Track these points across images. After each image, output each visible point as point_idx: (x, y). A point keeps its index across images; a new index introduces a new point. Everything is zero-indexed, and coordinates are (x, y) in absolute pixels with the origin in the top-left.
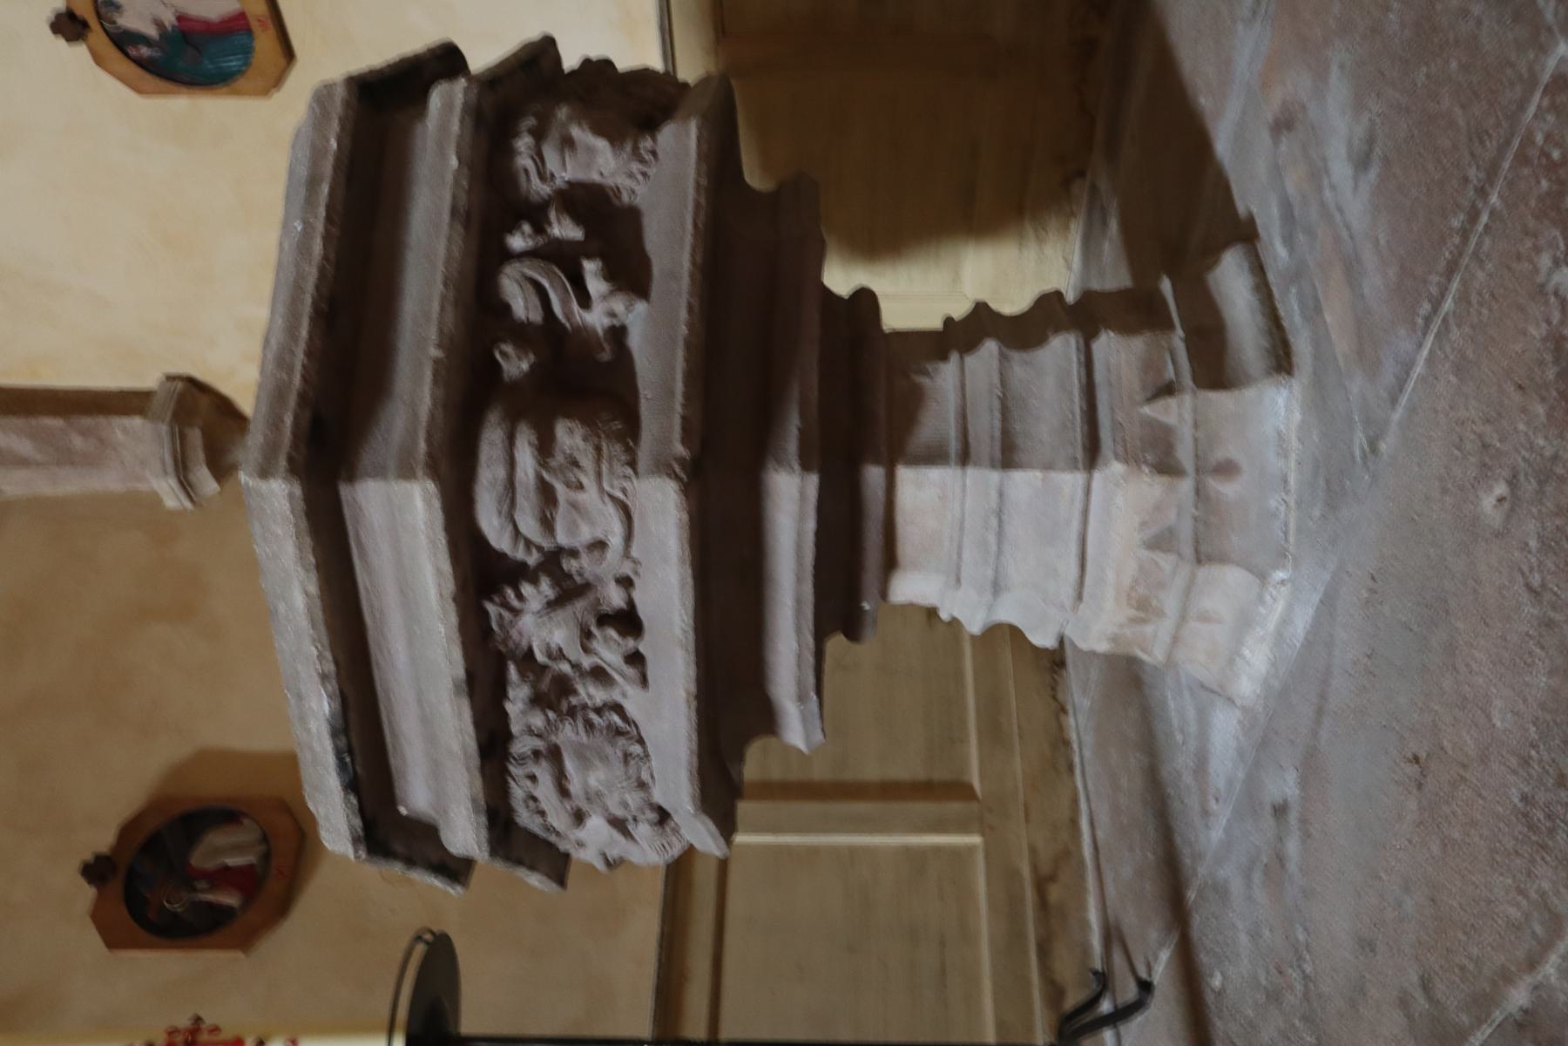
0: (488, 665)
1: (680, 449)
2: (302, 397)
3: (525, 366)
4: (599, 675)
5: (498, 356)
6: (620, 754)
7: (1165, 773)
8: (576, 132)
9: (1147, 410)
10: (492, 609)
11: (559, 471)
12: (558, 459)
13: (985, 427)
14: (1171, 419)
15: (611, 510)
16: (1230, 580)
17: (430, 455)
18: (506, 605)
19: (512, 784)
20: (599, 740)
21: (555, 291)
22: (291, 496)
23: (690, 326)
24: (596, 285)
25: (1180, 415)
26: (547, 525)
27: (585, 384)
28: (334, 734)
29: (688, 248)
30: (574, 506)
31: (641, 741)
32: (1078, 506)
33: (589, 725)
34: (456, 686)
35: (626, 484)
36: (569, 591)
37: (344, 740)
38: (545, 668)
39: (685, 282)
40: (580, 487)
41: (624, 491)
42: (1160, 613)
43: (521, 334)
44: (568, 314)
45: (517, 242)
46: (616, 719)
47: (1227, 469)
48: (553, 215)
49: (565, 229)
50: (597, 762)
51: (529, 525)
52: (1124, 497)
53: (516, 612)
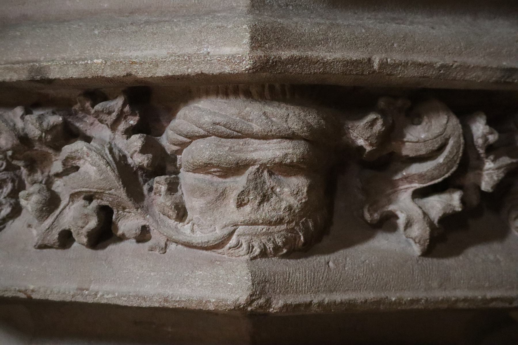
1: (277, 304)
3: (361, 142)
4: (51, 203)
5: (372, 116)
10: (117, 104)
11: (256, 182)
15: (219, 233)
17: (278, 62)
18: (121, 116)
21: (435, 168)
23: (399, 302)
24: (437, 205)
26: (204, 168)
27: (340, 192)
29: (470, 294)
30: (223, 195)
34: (39, 70)
36: (132, 181)
38: (58, 149)
39: (440, 295)
40: (240, 204)
41: (238, 245)
43: (391, 135)
44: (408, 179)
45: (480, 128)
48: (506, 160)
51: (202, 150)
53: (113, 127)
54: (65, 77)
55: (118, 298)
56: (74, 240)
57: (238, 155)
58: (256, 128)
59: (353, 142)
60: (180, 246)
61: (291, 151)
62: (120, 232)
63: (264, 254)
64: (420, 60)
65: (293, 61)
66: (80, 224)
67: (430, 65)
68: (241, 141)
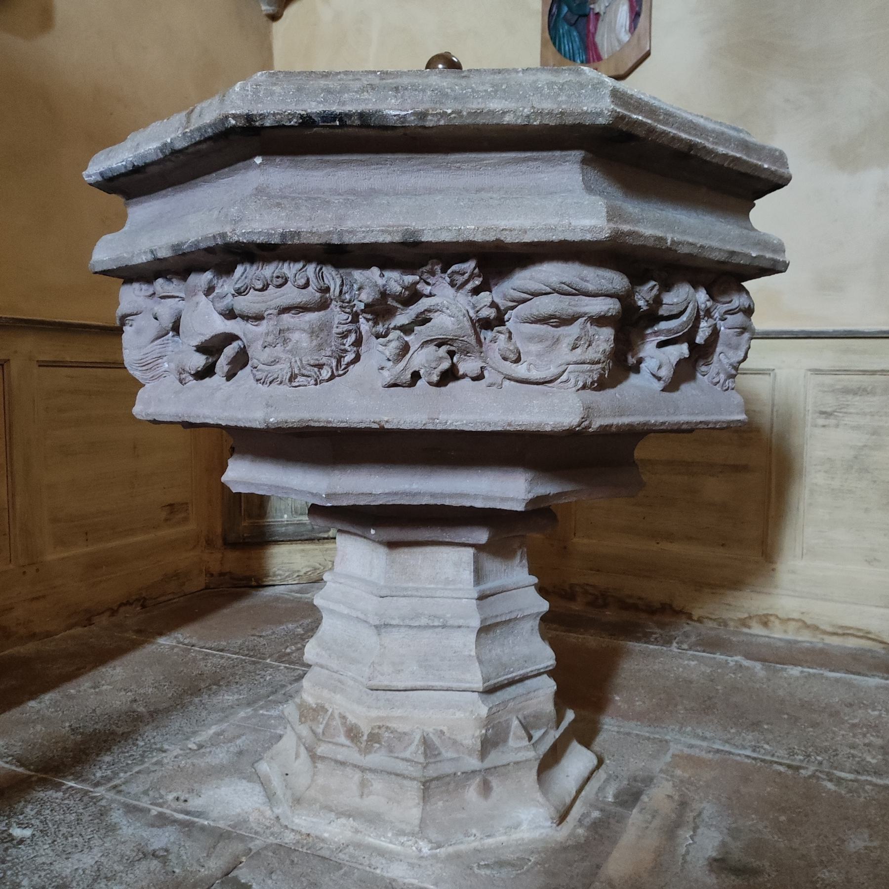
0: (413, 255)
1: (595, 425)
2: (651, 130)
3: (641, 303)
5: (653, 283)
6: (324, 360)
7: (150, 735)
9: (516, 722)
12: (592, 329)
13: (500, 608)
14: (512, 742)
15: (553, 371)
16: (410, 809)
18: (472, 277)
19: (299, 265)
22: (600, 114)
30: (557, 341)
31: (332, 377)
32: (455, 685)
33: (344, 335)
34: (414, 233)
35: (573, 381)
37: (357, 122)
40: (574, 348)
41: (567, 381)
42: (367, 751)
44: (656, 333)
46: (349, 357)
47: (486, 789)
50: (315, 343)
52: (460, 716)
54: (437, 240)
55: (466, 424)
56: (420, 378)
57: (575, 309)
58: (591, 287)
59: (635, 302)
60: (512, 383)
61: (612, 306)
62: (461, 373)
63: (584, 387)
65: (630, 234)
66: (434, 365)
68: (576, 298)
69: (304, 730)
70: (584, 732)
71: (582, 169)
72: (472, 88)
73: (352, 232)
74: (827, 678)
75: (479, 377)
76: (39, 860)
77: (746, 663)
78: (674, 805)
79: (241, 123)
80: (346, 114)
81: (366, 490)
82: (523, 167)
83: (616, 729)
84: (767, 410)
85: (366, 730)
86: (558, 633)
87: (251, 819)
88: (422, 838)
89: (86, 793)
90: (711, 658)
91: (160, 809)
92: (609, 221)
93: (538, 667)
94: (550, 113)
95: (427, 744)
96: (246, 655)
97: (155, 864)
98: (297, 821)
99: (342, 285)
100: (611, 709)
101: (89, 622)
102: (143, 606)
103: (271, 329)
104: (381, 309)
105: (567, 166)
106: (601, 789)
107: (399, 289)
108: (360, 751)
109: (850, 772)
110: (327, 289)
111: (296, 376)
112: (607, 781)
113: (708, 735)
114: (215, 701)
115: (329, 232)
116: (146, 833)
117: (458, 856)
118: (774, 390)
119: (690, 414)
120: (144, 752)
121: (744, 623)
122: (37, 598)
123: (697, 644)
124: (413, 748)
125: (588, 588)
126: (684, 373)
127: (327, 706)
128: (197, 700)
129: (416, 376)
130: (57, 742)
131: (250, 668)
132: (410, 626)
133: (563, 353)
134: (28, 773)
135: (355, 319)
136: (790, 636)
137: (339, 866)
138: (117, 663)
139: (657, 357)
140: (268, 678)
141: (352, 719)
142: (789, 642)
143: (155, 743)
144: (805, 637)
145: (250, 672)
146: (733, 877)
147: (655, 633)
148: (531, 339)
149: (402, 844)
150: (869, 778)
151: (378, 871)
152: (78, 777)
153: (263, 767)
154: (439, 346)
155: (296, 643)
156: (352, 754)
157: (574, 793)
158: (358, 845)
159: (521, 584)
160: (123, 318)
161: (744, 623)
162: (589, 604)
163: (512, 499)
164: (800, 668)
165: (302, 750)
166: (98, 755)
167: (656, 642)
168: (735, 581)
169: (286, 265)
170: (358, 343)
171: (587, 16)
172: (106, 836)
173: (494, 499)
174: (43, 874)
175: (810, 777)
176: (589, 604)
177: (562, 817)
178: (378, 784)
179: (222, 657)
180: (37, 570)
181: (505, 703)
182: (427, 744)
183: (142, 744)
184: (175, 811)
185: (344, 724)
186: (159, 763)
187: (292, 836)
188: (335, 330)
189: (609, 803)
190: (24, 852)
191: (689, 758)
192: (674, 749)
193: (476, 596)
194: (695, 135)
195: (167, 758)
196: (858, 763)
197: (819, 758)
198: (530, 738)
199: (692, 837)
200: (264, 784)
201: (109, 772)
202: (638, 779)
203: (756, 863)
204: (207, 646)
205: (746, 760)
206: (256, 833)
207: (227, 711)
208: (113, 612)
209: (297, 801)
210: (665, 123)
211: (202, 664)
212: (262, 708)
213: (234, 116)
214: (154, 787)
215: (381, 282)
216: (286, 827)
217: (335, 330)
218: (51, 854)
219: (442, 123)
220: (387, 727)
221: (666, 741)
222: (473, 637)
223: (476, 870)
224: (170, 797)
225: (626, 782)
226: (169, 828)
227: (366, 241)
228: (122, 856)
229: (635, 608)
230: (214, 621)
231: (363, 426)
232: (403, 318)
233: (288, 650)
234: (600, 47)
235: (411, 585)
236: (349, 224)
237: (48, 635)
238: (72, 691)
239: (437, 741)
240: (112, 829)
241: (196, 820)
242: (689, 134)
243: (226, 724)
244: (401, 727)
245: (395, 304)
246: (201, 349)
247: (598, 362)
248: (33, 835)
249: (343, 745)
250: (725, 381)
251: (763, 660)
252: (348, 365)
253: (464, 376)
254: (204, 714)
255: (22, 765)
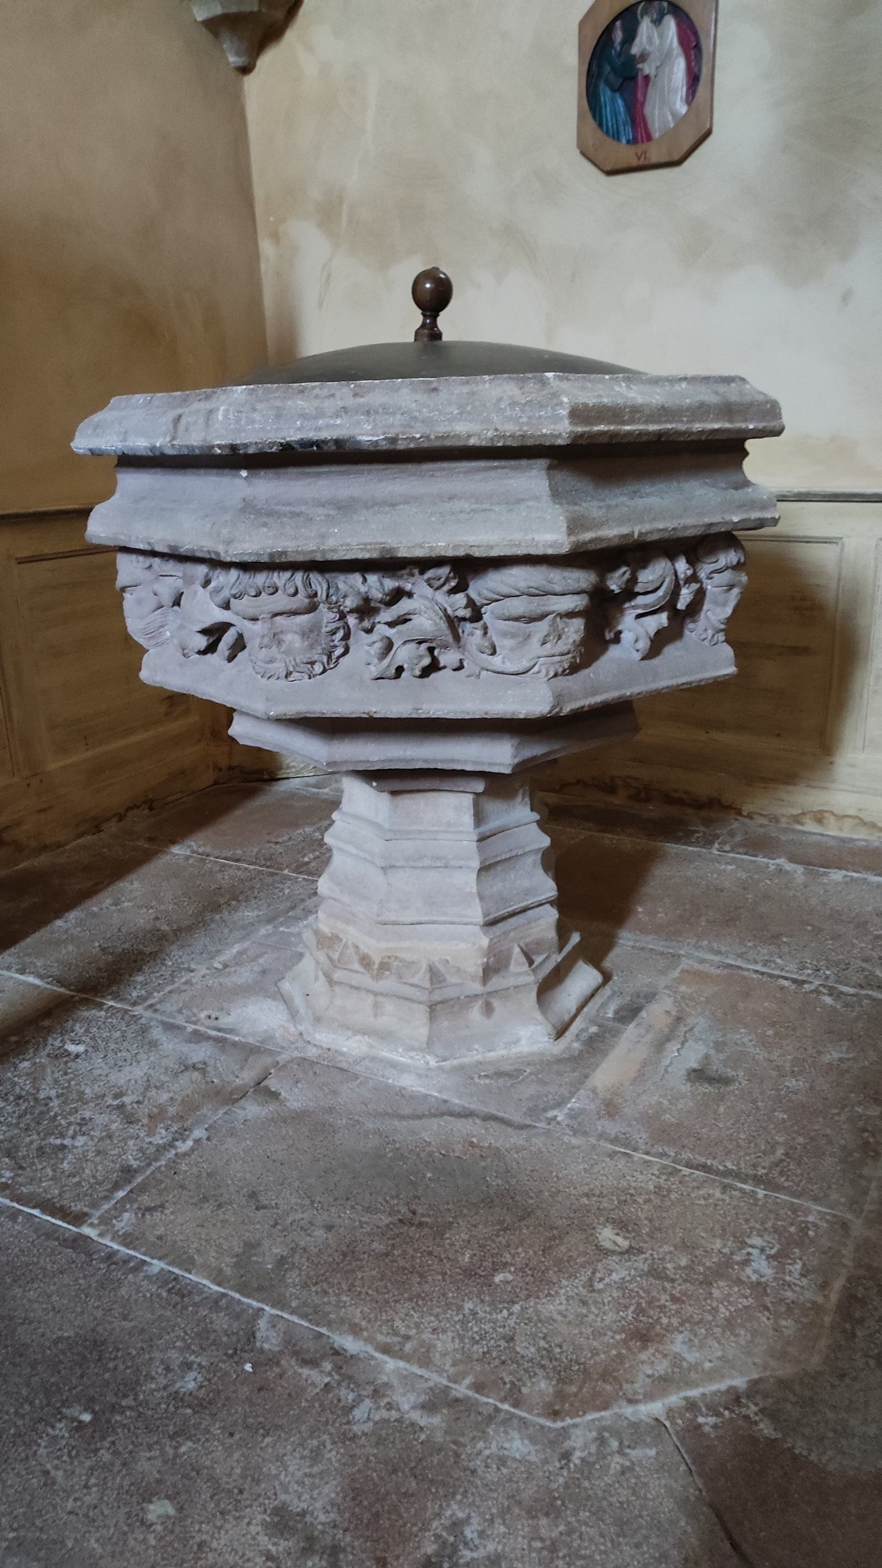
1: (567, 709)
3: (613, 587)
5: (624, 569)
6: (316, 657)
7: (176, 955)
8: (736, 591)
9: (517, 950)
11: (553, 623)
13: (499, 847)
14: (513, 968)
15: (525, 664)
16: (418, 1027)
18: (447, 580)
19: (287, 575)
20: (324, 641)
25: (520, 974)
28: (337, 442)
30: (529, 636)
32: (457, 919)
33: (333, 633)
34: (390, 550)
35: (544, 671)
40: (543, 644)
41: (538, 672)
42: (378, 977)
44: (634, 607)
46: (339, 651)
47: (488, 1009)
49: (686, 596)
50: (306, 643)
52: (462, 945)
58: (558, 589)
62: (442, 665)
63: (556, 675)
64: (661, 527)
65: (592, 541)
66: (415, 662)
67: (665, 530)
69: (322, 957)
70: (595, 953)
71: (548, 475)
72: (438, 410)
73: (334, 551)
74: (869, 884)
75: (460, 667)
76: (97, 1072)
77: (789, 866)
78: (669, 1021)
79: (227, 452)
80: (323, 441)
81: (362, 758)
82: (493, 474)
83: (631, 943)
84: (833, 585)
85: (377, 960)
86: (591, 833)
87: (277, 1035)
88: (430, 1053)
89: (126, 1012)
90: (752, 861)
91: (194, 1027)
92: (569, 535)
93: (539, 899)
94: (512, 436)
95: (434, 974)
96: (263, 866)
97: (196, 1075)
98: (318, 1037)
99: (329, 588)
100: (631, 922)
101: (98, 829)
102: (151, 809)
103: (266, 632)
104: (366, 609)
105: (534, 473)
106: (604, 1005)
107: (380, 596)
108: (372, 977)
109: (854, 987)
110: (316, 595)
111: (291, 673)
112: (610, 998)
113: (723, 949)
114: (236, 918)
115: (313, 551)
116: (186, 1048)
117: (462, 1068)
118: (841, 561)
119: (672, 678)
120: (173, 971)
121: (797, 819)
122: (44, 810)
123: (740, 845)
124: (421, 974)
125: (628, 780)
126: (659, 643)
127: (341, 936)
128: (217, 917)
129: (400, 670)
130: (90, 963)
131: (269, 880)
132: (414, 868)
133: (534, 646)
134: (72, 993)
135: (343, 616)
136: (845, 834)
137: (356, 1077)
138: (133, 876)
139: (635, 628)
140: (287, 891)
141: (364, 949)
142: (843, 840)
143: (182, 963)
144: (861, 835)
145: (268, 885)
146: (706, 1085)
147: (698, 832)
148: (504, 634)
149: (412, 1058)
150: (870, 993)
151: (390, 1081)
152: (116, 997)
153: (286, 986)
154: (420, 642)
155: (314, 851)
156: (366, 980)
157: (574, 1010)
158: (373, 1059)
159: (523, 822)
160: (123, 589)
161: (797, 819)
162: (630, 797)
163: (499, 764)
164: (844, 872)
165: (320, 974)
166: (130, 975)
167: (697, 843)
168: (789, 776)
169: (276, 574)
170: (346, 637)
171: (634, 78)
172: (149, 1051)
173: (483, 764)
174: (102, 1084)
175: (811, 992)
176: (630, 797)
177: (560, 1032)
178: (389, 1006)
179: (239, 868)
180: (41, 781)
181: (506, 933)
182: (434, 974)
183: (170, 963)
184: (208, 1028)
185: (357, 953)
186: (187, 982)
187: (314, 1050)
188: (324, 630)
189: (608, 1019)
190: (82, 1065)
191: (697, 974)
192: (685, 964)
193: (476, 838)
194: (666, 422)
195: (196, 978)
196: (866, 977)
197: (828, 972)
198: (531, 962)
199: (678, 1050)
200: (286, 1001)
201: (143, 992)
202: (642, 995)
203: (731, 1073)
204: (223, 855)
205: (755, 976)
206: (282, 1048)
207: (248, 929)
208: (121, 817)
209: (318, 1020)
210: (631, 422)
211: (219, 876)
212: (282, 924)
213: (219, 446)
214: (186, 1006)
215: (363, 589)
216: (309, 1042)
217: (324, 630)
218: (105, 1067)
219: (412, 446)
220: (396, 957)
221: (679, 956)
222: (474, 876)
223: (477, 1080)
224: (203, 1015)
225: (629, 998)
226: (204, 1043)
227: (347, 557)
228: (166, 1069)
229: (681, 802)
230: (228, 825)
231: (354, 716)
232: (387, 615)
233: (306, 859)
234: (649, 121)
235: (414, 828)
236: (331, 543)
237: (59, 845)
238: (95, 909)
239: (441, 968)
240: (154, 1045)
241: (228, 1036)
242: (659, 422)
243: (248, 943)
244: (409, 957)
245: (379, 605)
246: (204, 632)
247: (568, 653)
248: (86, 1051)
249: (357, 972)
250: (713, 636)
251: (806, 862)
252: (338, 658)
253: (444, 667)
254: (226, 931)
255: (62, 986)
